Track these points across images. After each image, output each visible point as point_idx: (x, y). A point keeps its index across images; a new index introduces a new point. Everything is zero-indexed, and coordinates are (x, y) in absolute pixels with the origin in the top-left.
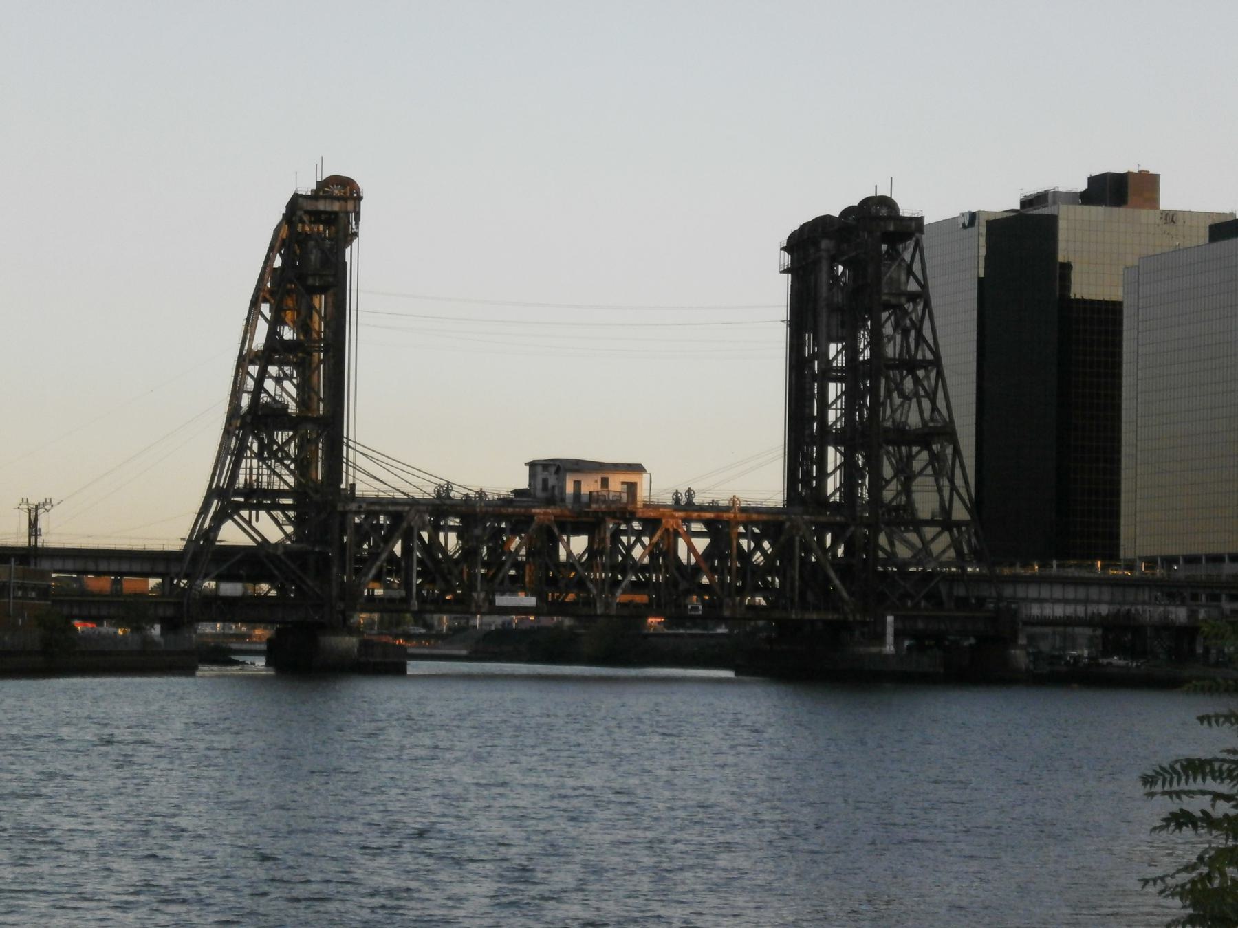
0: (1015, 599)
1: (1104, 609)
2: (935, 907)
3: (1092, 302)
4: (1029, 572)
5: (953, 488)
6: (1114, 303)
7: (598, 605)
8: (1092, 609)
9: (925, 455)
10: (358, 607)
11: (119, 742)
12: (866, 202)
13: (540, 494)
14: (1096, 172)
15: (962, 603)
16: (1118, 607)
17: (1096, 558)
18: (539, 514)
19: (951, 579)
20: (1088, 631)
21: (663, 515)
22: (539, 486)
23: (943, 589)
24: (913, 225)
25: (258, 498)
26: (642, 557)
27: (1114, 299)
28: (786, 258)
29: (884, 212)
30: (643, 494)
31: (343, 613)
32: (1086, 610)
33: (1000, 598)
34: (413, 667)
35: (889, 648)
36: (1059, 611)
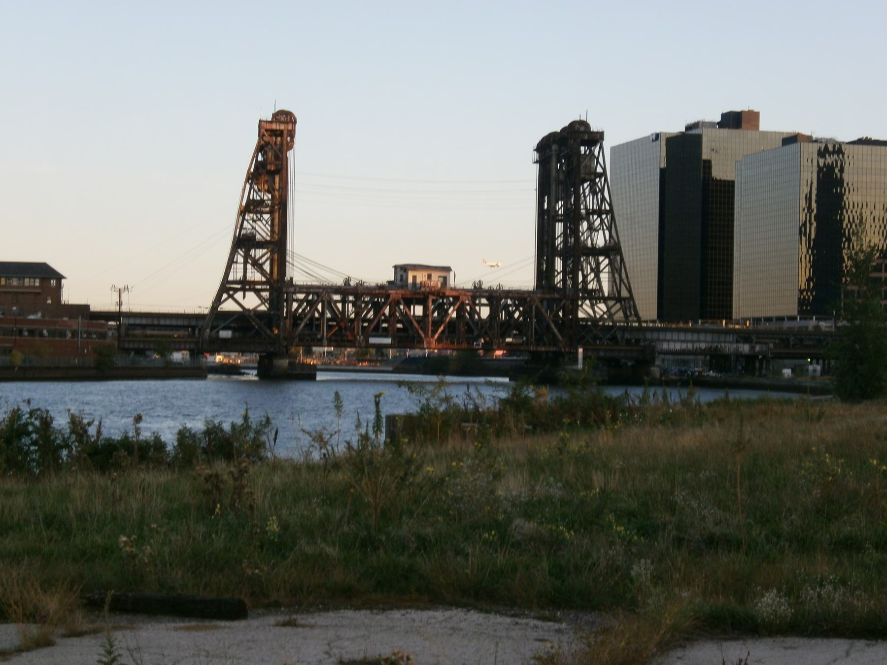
0: (651, 341)
1: (703, 346)
2: (852, 483)
3: (725, 181)
4: (686, 326)
5: (621, 280)
6: (729, 181)
7: (425, 343)
8: (696, 345)
9: (607, 261)
10: (294, 344)
11: (266, 413)
12: (573, 124)
13: (398, 282)
14: (726, 111)
15: (628, 342)
16: (710, 344)
17: (722, 319)
18: (393, 293)
19: (623, 329)
20: (702, 357)
21: (461, 294)
22: (399, 278)
23: (619, 336)
24: (598, 136)
25: (246, 285)
26: (519, 317)
27: (729, 179)
28: (536, 156)
29: (582, 129)
30: (451, 283)
31: (286, 347)
32: (693, 346)
33: (645, 340)
34: (320, 376)
35: (580, 366)
36: (678, 346)
